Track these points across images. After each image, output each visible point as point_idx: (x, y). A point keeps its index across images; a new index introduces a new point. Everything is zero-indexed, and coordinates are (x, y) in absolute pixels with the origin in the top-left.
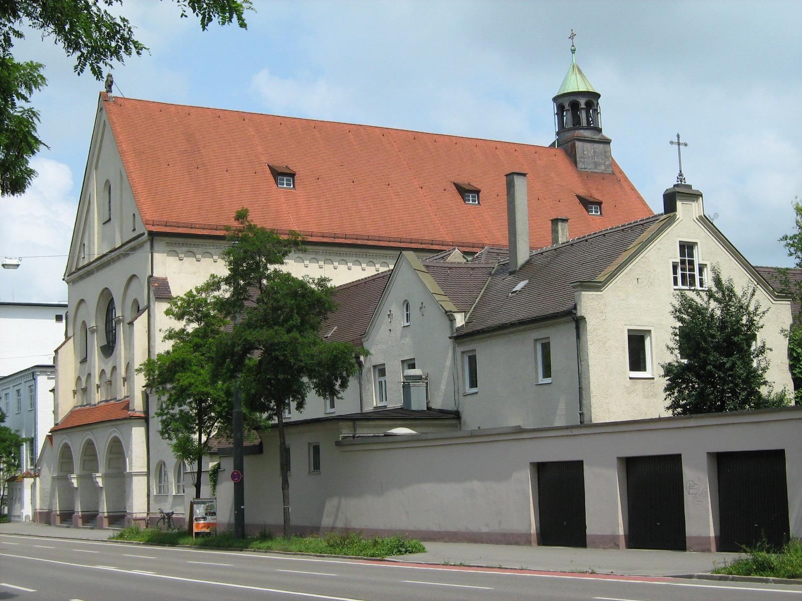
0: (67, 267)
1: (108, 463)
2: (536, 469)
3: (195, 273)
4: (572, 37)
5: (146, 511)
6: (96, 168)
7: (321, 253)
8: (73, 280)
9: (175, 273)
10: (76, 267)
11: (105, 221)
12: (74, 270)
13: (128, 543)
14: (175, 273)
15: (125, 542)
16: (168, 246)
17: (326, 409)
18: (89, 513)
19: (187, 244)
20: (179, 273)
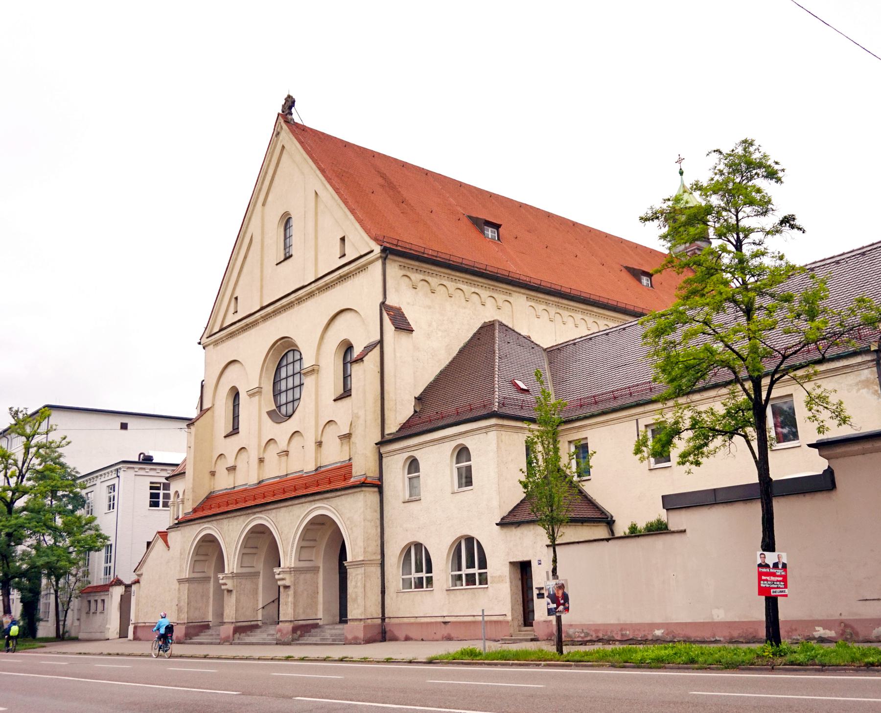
0: (206, 328)
1: (298, 554)
2: (519, 571)
3: (430, 307)
4: (680, 161)
5: (380, 616)
6: (264, 205)
7: (551, 305)
8: (215, 341)
9: (408, 304)
10: (222, 324)
11: (278, 262)
12: (216, 329)
13: (513, 664)
14: (408, 304)
15: (513, 664)
16: (401, 269)
17: (649, 465)
18: (199, 624)
19: (421, 271)
20: (413, 305)
